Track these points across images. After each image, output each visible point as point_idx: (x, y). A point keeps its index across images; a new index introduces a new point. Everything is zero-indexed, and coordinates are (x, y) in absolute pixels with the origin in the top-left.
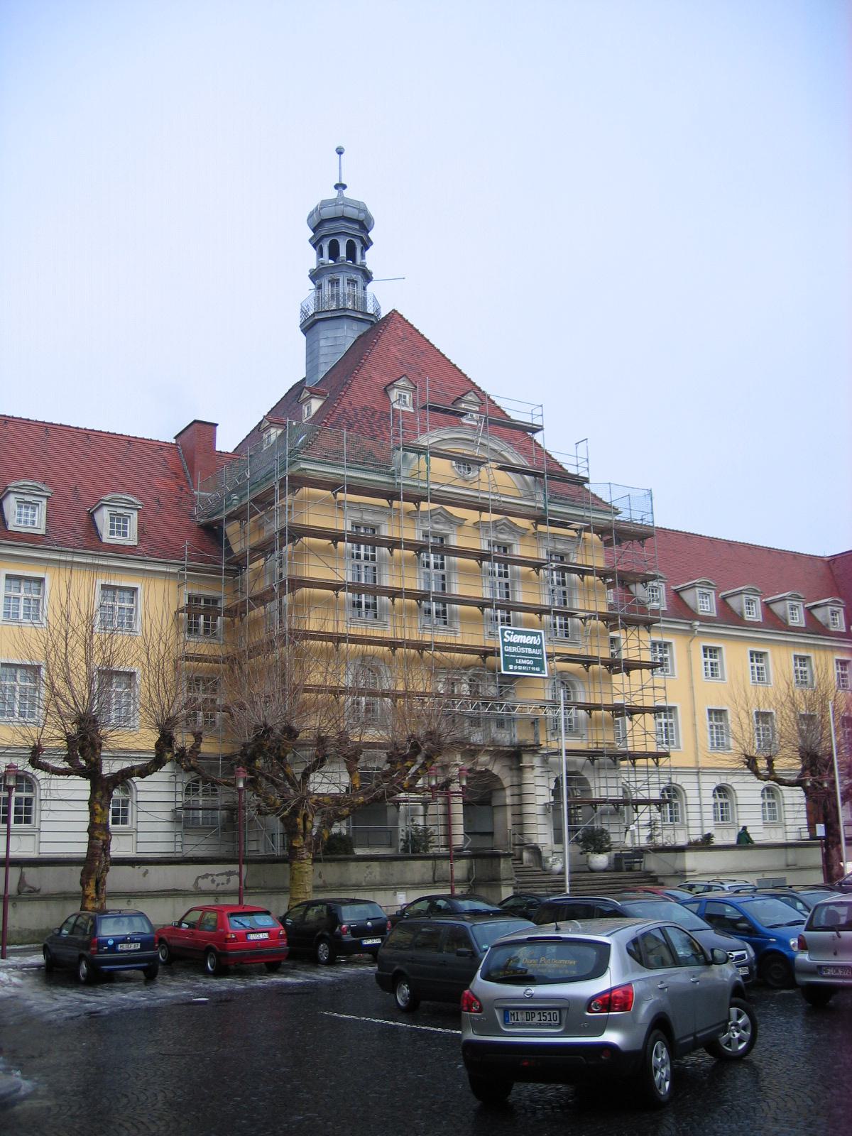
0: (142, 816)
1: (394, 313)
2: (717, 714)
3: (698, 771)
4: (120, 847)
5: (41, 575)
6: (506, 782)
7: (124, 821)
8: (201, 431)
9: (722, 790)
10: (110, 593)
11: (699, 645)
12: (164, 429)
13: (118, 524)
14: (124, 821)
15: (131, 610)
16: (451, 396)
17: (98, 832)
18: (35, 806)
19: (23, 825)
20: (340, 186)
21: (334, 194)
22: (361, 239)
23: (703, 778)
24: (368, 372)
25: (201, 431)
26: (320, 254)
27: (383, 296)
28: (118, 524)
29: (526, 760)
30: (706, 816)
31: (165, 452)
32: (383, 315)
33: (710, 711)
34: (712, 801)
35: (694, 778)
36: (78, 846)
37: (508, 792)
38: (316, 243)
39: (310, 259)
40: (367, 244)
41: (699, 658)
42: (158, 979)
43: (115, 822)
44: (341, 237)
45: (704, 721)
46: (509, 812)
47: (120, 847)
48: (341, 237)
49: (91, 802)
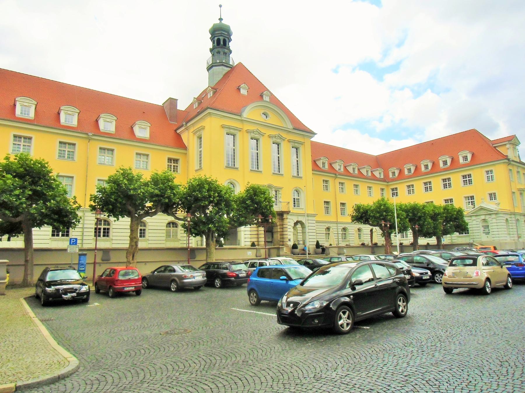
0: (150, 235)
1: (240, 64)
2: (343, 204)
3: (337, 223)
4: (142, 244)
5: (113, 148)
6: (278, 224)
7: (144, 236)
8: (172, 102)
9: (344, 229)
11: (338, 181)
12: (160, 101)
13: (142, 131)
14: (144, 236)
15: (147, 162)
16: (259, 92)
17: (133, 239)
18: (111, 231)
19: (106, 238)
20: (221, 19)
21: (218, 22)
22: (228, 38)
23: (339, 225)
24: (231, 83)
25: (172, 102)
26: (214, 43)
27: (235, 59)
28: (142, 131)
29: (285, 216)
30: (339, 237)
31: (133, 223)
32: (235, 65)
33: (341, 203)
34: (341, 233)
35: (335, 225)
36: (126, 244)
37: (279, 227)
38: (212, 39)
39: (210, 45)
40: (230, 40)
41: (338, 186)
42: (142, 293)
43: (141, 236)
44: (221, 39)
45: (339, 207)
46: (279, 234)
47: (142, 244)
48: (221, 39)
49: (131, 227)
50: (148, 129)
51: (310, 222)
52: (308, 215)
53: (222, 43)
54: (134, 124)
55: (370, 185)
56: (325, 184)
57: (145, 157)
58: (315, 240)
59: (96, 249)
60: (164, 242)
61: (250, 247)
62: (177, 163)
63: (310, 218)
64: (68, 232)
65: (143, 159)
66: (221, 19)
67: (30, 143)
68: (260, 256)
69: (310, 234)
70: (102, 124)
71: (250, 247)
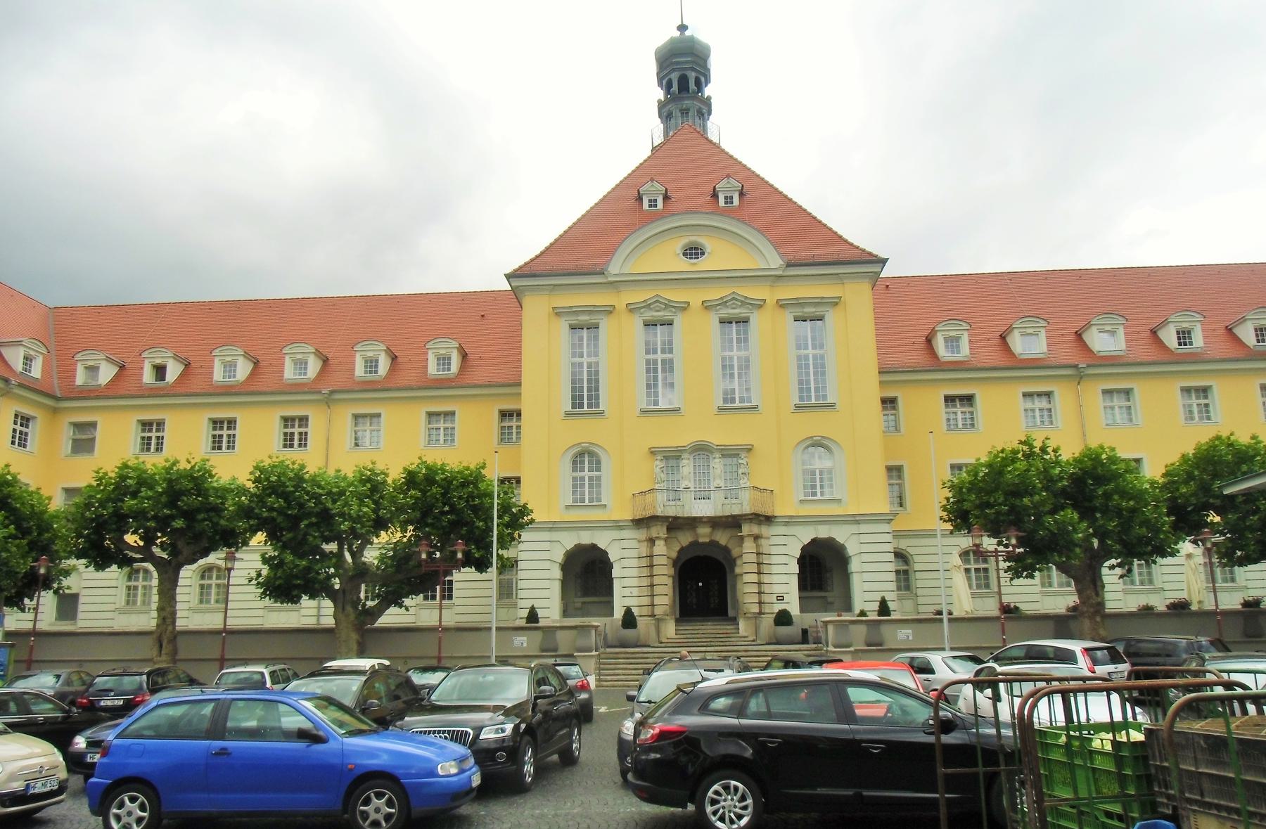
0: (1166, 578)
10: (1028, 399)
15: (1050, 410)
20: (682, 28)
21: (677, 34)
38: (660, 84)
44: (683, 76)
48: (683, 76)
50: (1043, 333)
51: (864, 538)
52: (856, 520)
53: (692, 86)
54: (1010, 329)
55: (26, 410)
56: (18, 428)
57: (1044, 399)
58: (878, 597)
59: (225, 630)
60: (1037, 597)
61: (523, 623)
62: (1206, 397)
63: (864, 528)
64: (1150, 574)
65: (1118, 402)
66: (682, 28)
67: (453, 421)
68: (556, 650)
69: (866, 577)
70: (1018, 344)
71: (523, 623)
